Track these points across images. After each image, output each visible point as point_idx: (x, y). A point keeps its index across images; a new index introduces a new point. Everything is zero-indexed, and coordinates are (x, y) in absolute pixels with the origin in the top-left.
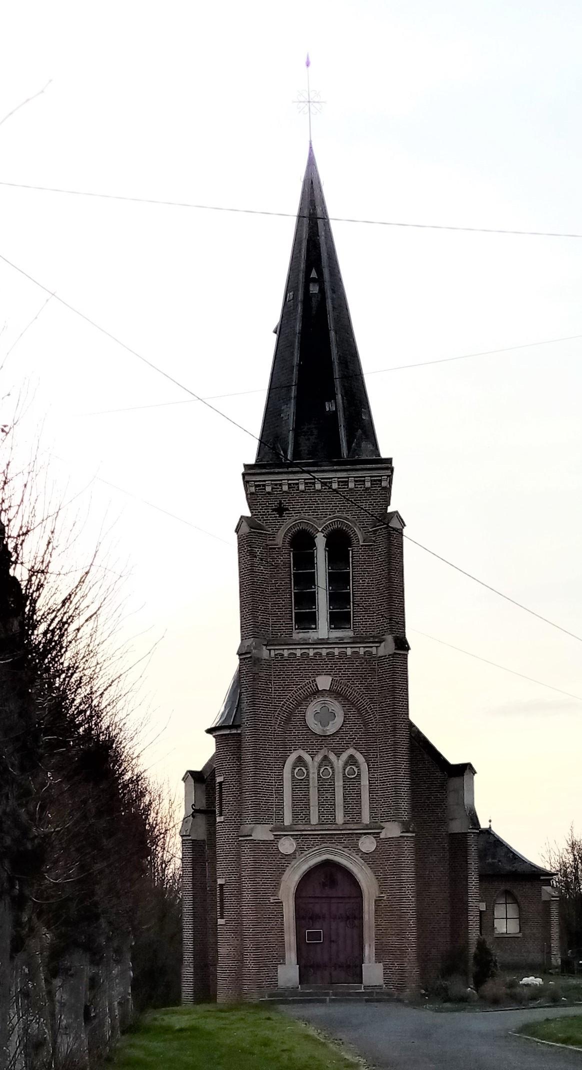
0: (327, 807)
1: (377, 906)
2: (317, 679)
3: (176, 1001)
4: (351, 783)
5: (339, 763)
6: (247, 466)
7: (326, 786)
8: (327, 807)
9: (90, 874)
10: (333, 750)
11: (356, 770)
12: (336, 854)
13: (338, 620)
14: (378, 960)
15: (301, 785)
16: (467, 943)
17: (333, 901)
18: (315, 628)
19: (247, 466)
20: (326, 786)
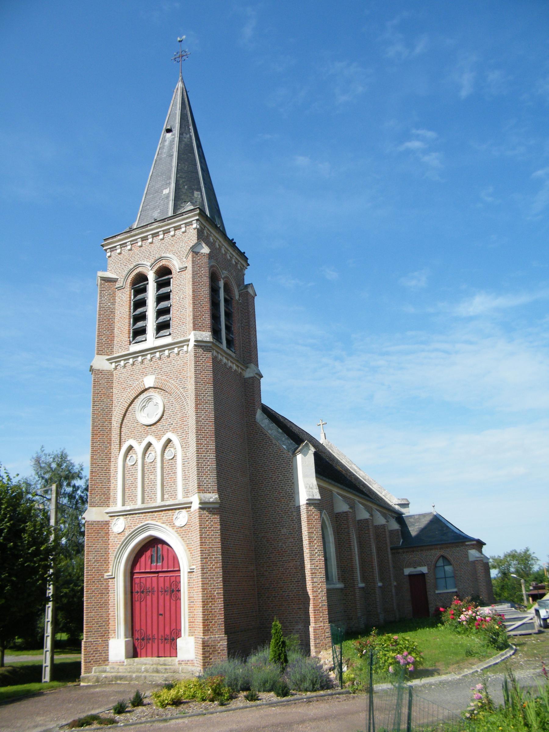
4: (167, 467)
5: (158, 446)
17: (160, 575)
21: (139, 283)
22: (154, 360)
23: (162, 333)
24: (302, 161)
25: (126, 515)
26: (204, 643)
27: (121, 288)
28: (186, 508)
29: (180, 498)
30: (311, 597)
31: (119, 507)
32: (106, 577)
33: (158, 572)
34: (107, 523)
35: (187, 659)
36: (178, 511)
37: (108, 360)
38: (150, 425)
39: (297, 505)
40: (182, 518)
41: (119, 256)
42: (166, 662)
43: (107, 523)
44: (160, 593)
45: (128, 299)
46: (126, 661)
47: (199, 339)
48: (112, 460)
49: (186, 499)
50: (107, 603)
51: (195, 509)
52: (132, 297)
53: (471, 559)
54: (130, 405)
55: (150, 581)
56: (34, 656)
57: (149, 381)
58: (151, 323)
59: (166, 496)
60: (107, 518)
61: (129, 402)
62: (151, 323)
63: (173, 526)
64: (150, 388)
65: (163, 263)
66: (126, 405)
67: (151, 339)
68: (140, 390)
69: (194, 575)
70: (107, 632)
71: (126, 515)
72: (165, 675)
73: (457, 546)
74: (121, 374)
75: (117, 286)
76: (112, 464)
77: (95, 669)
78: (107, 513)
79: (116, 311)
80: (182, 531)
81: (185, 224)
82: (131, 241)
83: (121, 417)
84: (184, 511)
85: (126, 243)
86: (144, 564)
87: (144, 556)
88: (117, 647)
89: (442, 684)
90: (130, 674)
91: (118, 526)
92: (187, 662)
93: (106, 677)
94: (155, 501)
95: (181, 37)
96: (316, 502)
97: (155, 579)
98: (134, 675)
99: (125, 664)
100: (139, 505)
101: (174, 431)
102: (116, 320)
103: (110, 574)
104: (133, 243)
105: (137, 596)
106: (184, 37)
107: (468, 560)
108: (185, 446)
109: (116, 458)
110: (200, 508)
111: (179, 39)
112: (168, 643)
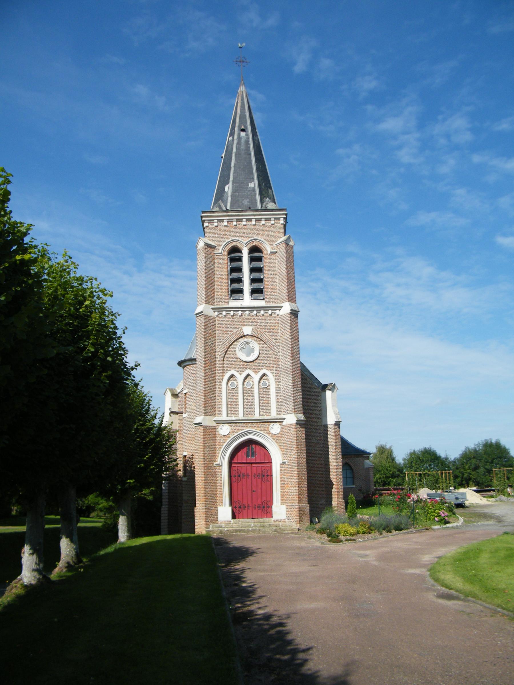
0: (248, 407)
1: (281, 468)
2: (243, 328)
3: (256, 373)
4: (264, 392)
5: (256, 377)
6: (414, 451)
7: (248, 392)
8: (248, 407)
9: (152, 424)
10: (253, 371)
11: (267, 382)
12: (255, 433)
13: (256, 292)
14: (283, 503)
15: (232, 393)
16: (326, 427)
17: (253, 465)
18: (243, 299)
19: (414, 451)
20: (248, 392)
21: (234, 252)
22: (251, 315)
23: (255, 295)
24: (142, 90)
25: (231, 423)
26: (299, 508)
27: (218, 255)
28: (279, 422)
29: (274, 414)
30: (334, 483)
31: (224, 417)
32: (215, 465)
33: (251, 463)
34: (214, 428)
35: (280, 519)
36: (272, 424)
37: (213, 309)
38: (249, 362)
39: (323, 424)
40: (275, 429)
41: (216, 228)
42: (265, 521)
43: (214, 428)
44: (253, 477)
45: (226, 265)
46: (232, 520)
47: (293, 309)
48: (217, 383)
49: (279, 416)
50: (215, 483)
51: (289, 423)
52: (229, 263)
53: (366, 466)
54: (231, 345)
55: (245, 469)
56: (203, 515)
57: (247, 330)
58: (247, 286)
59: (262, 413)
60: (214, 424)
61: (230, 342)
62: (247, 286)
63: (269, 433)
64: (248, 335)
65: (256, 243)
66: (228, 345)
67: (247, 300)
68: (239, 336)
69: (285, 467)
70: (216, 502)
71: (231, 423)
72: (274, 528)
73: (358, 457)
74: (223, 321)
75: (215, 252)
76: (217, 386)
77: (212, 526)
78: (215, 421)
79: (216, 272)
80: (276, 437)
81: (275, 218)
82: (227, 219)
83: (224, 352)
84: (277, 423)
85: (223, 220)
86: (241, 456)
87: (241, 452)
88: (225, 512)
89: (453, 527)
90: (247, 528)
91: (224, 430)
92: (280, 521)
93: (228, 530)
94: (254, 414)
95: (241, 44)
96: (302, 422)
97: (249, 468)
98: (250, 529)
99: (232, 522)
100: (241, 416)
101: (268, 368)
102: (216, 279)
103: (218, 463)
104: (230, 221)
105: (234, 479)
106: (244, 44)
107: (364, 467)
108: (278, 380)
109: (221, 382)
110: (296, 423)
111: (240, 45)
112: (265, 508)
